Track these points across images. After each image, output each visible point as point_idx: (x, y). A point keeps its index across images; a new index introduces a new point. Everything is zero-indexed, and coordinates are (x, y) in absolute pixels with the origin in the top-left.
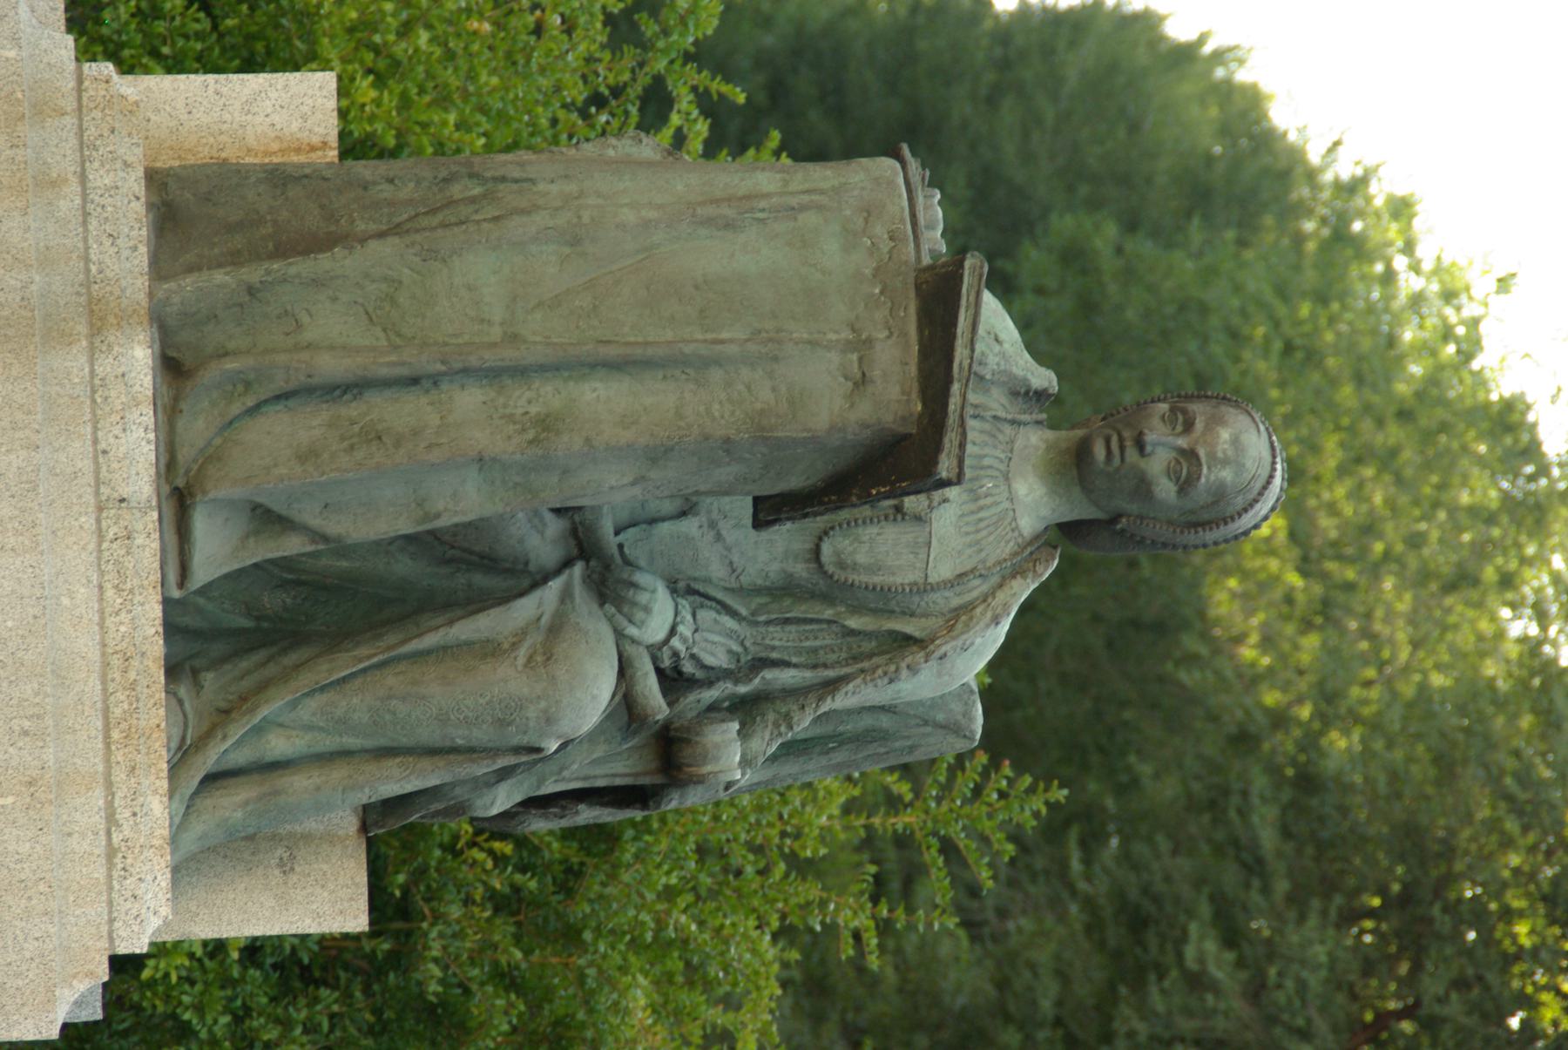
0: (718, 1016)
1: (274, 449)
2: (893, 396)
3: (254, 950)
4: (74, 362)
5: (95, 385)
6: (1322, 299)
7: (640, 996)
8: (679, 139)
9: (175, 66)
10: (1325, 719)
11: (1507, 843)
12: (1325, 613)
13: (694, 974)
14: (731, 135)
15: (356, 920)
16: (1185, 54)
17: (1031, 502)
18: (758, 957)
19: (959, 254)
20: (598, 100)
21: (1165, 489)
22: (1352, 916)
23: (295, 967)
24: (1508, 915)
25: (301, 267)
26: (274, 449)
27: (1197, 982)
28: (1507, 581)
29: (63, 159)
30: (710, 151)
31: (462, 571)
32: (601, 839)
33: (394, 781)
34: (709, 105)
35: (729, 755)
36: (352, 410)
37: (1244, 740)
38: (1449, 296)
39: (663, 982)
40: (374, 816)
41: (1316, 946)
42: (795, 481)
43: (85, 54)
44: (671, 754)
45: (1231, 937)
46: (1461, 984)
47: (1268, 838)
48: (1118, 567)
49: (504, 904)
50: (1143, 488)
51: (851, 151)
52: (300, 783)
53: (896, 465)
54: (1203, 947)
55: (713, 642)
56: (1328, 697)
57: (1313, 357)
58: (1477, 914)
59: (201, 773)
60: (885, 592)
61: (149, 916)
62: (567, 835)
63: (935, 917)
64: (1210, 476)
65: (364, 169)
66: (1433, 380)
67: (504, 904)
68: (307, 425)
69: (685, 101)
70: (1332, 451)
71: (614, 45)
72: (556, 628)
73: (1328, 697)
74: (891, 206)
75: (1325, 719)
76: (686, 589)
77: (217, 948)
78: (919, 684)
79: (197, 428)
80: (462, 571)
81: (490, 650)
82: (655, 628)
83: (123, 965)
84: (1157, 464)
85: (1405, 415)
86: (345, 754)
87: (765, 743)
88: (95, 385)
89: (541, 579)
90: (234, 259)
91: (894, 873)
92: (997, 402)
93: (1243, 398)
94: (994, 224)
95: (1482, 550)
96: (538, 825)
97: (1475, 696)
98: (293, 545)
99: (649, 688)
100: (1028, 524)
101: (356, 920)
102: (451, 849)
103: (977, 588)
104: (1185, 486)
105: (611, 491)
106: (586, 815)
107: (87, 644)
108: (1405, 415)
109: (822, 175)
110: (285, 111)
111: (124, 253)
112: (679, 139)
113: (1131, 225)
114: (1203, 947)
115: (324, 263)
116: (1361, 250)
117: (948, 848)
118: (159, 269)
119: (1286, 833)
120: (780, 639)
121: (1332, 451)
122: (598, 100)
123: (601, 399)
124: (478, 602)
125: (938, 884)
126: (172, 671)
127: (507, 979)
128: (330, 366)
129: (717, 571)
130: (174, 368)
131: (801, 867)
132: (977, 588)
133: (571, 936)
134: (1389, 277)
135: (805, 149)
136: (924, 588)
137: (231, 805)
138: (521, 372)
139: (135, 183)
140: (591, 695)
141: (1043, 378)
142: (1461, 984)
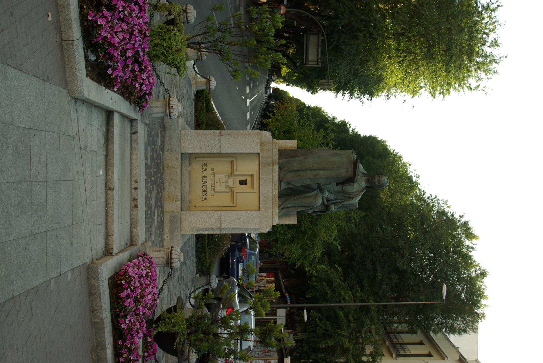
0: (331, 233)
1: (290, 176)
2: (350, 173)
3: (286, 225)
4: (271, 168)
5: (273, 170)
6: (392, 166)
7: (323, 231)
8: (330, 148)
9: (281, 140)
10: (391, 207)
11: (408, 219)
12: (391, 197)
13: (328, 229)
14: (335, 147)
15: (296, 223)
16: (380, 141)
17: (364, 184)
18: (335, 228)
19: (357, 160)
20: (322, 144)
21: (377, 183)
22: (393, 226)
23: (289, 227)
24: (408, 226)
25: (293, 159)
26: (290, 176)
27: (377, 232)
28: (409, 194)
29: (270, 148)
30: (333, 149)
31: (307, 189)
32: (320, 216)
33: (300, 209)
34: (333, 144)
35: (333, 208)
36: (297, 173)
37: (383, 209)
38: (404, 166)
39: (325, 230)
40: (298, 213)
41: (389, 228)
42: (340, 181)
43: (273, 138)
44: (327, 208)
45: (381, 228)
46: (403, 233)
47: (385, 218)
48: (372, 189)
49: (310, 222)
50: (375, 183)
51: (346, 149)
52: (291, 209)
53: (351, 180)
54: (378, 228)
55: (332, 197)
56: (392, 205)
57: (391, 171)
58: (405, 226)
59: (282, 208)
60: (349, 193)
61: (276, 221)
62: (317, 215)
63: (352, 225)
64: (381, 182)
65: (299, 150)
66: (403, 174)
67: (310, 222)
68: (293, 174)
69: (330, 144)
70: (393, 180)
71: (324, 138)
72: (316, 195)
73: (392, 205)
74: (352, 155)
75: (391, 207)
76: (329, 191)
77: (282, 225)
78: (352, 202)
79: (282, 174)
80: (307, 189)
81: (310, 197)
82: (326, 195)
83: (273, 226)
84: (376, 181)
85: (400, 177)
86: (295, 207)
87: (336, 207)
88: (273, 170)
89: (315, 190)
90: (286, 158)
91: (349, 220)
92: (360, 174)
93: (385, 175)
94: (360, 156)
95: (407, 191)
96: (314, 214)
97: (406, 205)
98: (291, 186)
99: (325, 201)
100: (363, 186)
101: (296, 223)
102: (305, 216)
103: (358, 192)
104: (379, 183)
105: (322, 182)
106: (319, 213)
107: (271, 195)
108: (400, 177)
109: (344, 151)
110: (292, 144)
111: (276, 158)
112: (330, 148)
113: (374, 158)
114: (378, 228)
115: (295, 159)
116: (396, 161)
117: (354, 218)
118: (279, 159)
119: (387, 218)
120: (338, 197)
121: (393, 180)
122: (322, 144)
123: (321, 173)
124: (308, 192)
125: (353, 221)
126: (279, 198)
127: (310, 229)
128: (295, 169)
129: (332, 190)
130: (280, 168)
131: (339, 219)
132: (358, 192)
133: (317, 225)
134: (399, 164)
135: (342, 149)
136: (353, 192)
137: (284, 211)
138: (313, 170)
139: (277, 151)
140: (320, 202)
141: (365, 172)
142: (403, 233)
